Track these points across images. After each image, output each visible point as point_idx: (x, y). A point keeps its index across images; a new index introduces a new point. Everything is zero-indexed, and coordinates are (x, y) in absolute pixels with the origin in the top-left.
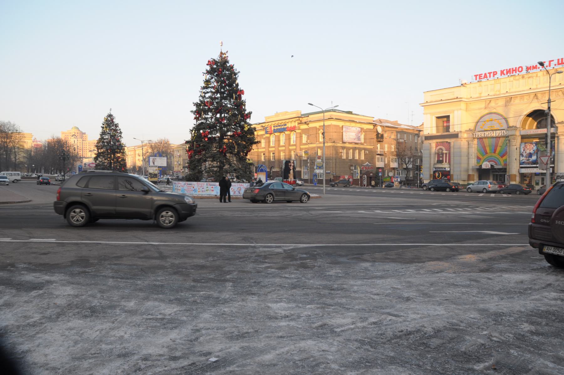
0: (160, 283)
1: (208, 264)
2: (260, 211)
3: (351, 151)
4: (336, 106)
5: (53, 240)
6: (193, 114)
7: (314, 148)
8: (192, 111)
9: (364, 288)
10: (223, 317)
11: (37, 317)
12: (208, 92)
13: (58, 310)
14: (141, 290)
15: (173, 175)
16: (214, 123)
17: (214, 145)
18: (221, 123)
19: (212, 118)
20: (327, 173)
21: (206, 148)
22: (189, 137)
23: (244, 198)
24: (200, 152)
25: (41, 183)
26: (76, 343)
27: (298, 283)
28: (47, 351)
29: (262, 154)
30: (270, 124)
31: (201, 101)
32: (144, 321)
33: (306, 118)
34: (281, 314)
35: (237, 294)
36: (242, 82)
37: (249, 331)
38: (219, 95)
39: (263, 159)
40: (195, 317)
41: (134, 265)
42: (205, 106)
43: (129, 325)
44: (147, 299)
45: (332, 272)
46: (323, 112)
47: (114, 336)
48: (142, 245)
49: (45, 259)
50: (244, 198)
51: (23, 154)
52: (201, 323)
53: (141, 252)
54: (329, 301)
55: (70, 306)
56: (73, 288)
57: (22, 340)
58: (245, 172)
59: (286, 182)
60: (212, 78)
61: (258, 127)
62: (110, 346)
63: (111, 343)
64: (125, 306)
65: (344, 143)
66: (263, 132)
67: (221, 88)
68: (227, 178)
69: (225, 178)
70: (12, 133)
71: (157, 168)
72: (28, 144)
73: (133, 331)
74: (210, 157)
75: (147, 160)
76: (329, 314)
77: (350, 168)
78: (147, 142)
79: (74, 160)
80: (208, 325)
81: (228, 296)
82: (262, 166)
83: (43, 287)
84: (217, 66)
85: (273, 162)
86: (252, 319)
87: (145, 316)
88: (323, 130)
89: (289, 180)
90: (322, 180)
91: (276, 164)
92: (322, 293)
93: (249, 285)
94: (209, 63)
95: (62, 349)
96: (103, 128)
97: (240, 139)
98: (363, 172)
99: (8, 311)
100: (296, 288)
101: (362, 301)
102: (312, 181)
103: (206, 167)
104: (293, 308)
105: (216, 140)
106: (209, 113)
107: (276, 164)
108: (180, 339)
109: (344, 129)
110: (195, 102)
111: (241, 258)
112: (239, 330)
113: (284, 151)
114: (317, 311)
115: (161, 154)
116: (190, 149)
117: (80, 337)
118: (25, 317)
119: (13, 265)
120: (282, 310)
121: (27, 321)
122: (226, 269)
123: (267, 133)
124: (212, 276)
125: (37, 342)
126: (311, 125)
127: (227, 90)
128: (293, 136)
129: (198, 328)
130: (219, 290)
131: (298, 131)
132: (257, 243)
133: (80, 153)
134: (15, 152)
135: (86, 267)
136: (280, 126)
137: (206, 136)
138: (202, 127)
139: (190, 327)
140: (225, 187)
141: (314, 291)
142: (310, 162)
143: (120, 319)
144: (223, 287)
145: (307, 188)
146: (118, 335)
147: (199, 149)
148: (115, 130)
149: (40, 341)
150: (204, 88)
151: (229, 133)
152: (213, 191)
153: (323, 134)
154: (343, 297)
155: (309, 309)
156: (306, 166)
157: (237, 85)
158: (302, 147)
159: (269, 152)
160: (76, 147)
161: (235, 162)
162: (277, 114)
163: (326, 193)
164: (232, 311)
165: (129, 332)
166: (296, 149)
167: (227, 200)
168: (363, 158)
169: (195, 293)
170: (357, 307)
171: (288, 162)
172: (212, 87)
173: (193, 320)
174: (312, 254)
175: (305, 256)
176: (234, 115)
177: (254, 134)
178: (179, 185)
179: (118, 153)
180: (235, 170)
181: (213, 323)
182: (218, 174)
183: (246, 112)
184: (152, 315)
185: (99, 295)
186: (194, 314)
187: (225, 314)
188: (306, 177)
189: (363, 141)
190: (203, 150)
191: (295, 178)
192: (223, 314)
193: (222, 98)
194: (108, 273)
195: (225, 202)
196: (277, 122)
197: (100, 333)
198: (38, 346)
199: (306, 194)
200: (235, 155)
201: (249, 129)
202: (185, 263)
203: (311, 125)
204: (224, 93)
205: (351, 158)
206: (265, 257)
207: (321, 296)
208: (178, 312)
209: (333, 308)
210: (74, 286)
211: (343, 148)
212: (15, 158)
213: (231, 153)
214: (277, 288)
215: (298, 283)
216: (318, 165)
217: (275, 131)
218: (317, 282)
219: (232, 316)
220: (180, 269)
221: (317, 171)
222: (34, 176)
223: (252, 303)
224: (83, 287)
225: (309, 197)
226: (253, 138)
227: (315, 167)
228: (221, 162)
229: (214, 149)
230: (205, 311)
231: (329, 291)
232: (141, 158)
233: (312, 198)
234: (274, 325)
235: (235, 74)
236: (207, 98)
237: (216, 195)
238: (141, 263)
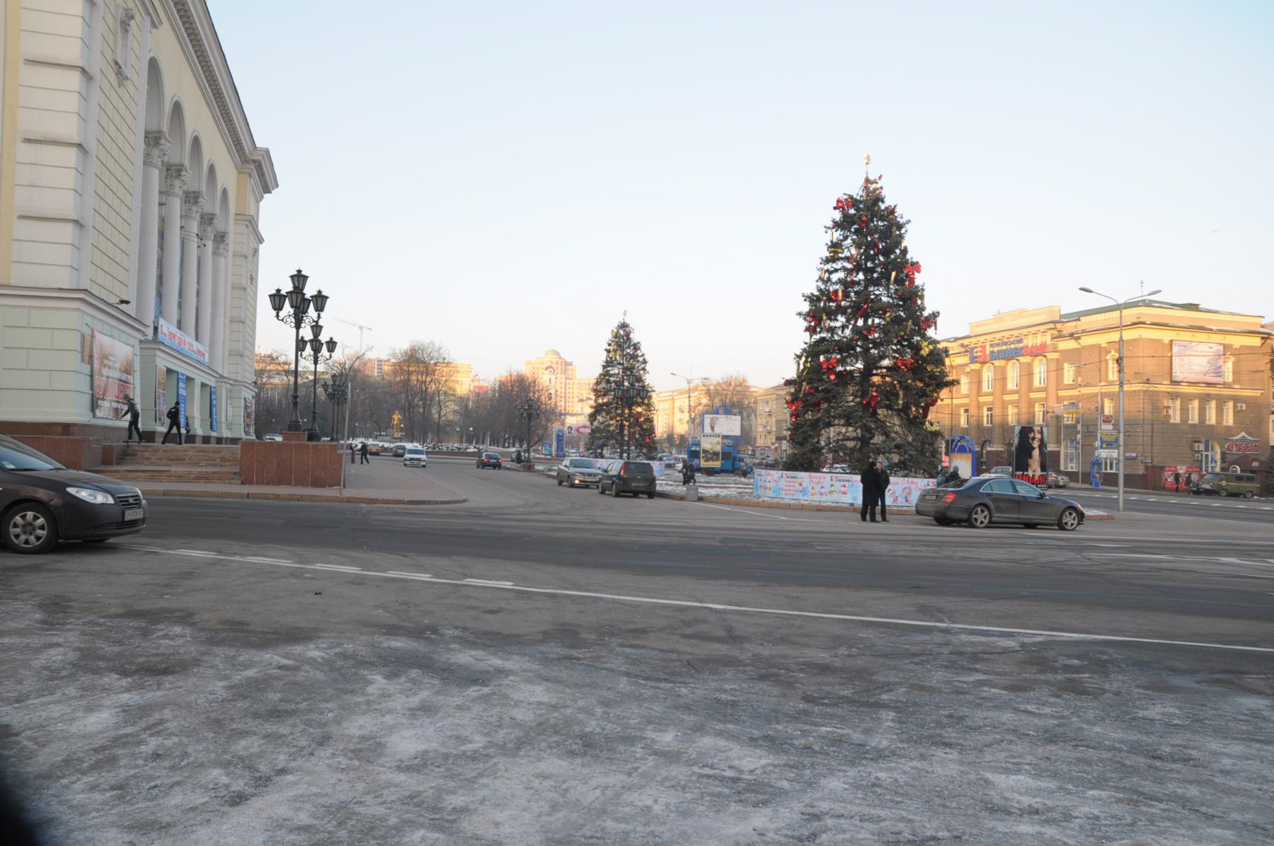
0: (729, 698)
1: (838, 663)
2: (957, 544)
3: (1196, 403)
4: (1154, 293)
5: (508, 585)
6: (801, 320)
7: (1095, 395)
8: (800, 314)
9: (1254, 766)
10: (874, 793)
11: (479, 742)
12: (836, 270)
13: (519, 733)
14: (687, 708)
15: (753, 455)
16: (852, 339)
17: (851, 389)
18: (865, 339)
19: (844, 327)
20: (1127, 459)
21: (831, 396)
22: (791, 371)
23: (918, 512)
24: (816, 405)
25: (483, 465)
26: (554, 807)
27: (1061, 730)
28: (500, 816)
29: (962, 410)
30: (982, 339)
31: (820, 290)
32: (694, 778)
33: (1074, 324)
34: (1018, 802)
35: (908, 741)
36: (915, 245)
37: (940, 834)
38: (861, 276)
39: (963, 422)
40: (810, 784)
41: (672, 651)
42: (830, 300)
43: (662, 783)
44: (700, 729)
45: (1154, 712)
46: (1118, 307)
47: (631, 804)
48: (688, 608)
49: (493, 623)
50: (918, 512)
51: (453, 406)
52: (823, 799)
53: (688, 624)
54: (1148, 786)
55: (541, 727)
56: (547, 690)
57: (453, 784)
58: (922, 454)
59: (1022, 477)
60: (846, 238)
61: (954, 348)
62: (623, 825)
63: (624, 820)
64: (654, 741)
65: (1174, 383)
66: (964, 360)
67: (867, 260)
68: (878, 466)
69: (874, 464)
70: (435, 364)
71: (720, 439)
72: (463, 386)
73: (672, 798)
74: (840, 417)
75: (697, 421)
76: (1152, 822)
77: (1191, 447)
78: (699, 382)
79: (548, 420)
80: (839, 808)
81: (885, 743)
82: (962, 438)
83: (489, 680)
84: (858, 210)
85: (988, 429)
86: (945, 806)
87: (696, 769)
88: (1119, 351)
89: (1030, 473)
90: (1116, 475)
91: (997, 435)
92: (1128, 762)
93: (937, 723)
94: (840, 205)
95: (527, 816)
96: (608, 351)
97: (910, 375)
98: (1229, 458)
99: (428, 721)
100: (1056, 743)
101: (1252, 802)
102: (1086, 478)
103: (829, 438)
104: (1051, 792)
105: (853, 377)
106: (839, 317)
107: (997, 435)
108: (776, 831)
109: (1175, 349)
110: (808, 292)
111: (915, 655)
112: (913, 829)
113: (1016, 404)
114: (1117, 809)
115: (728, 409)
116: (794, 399)
117: (562, 796)
118: (458, 738)
119: (434, 630)
120: (1021, 794)
121: (462, 748)
122: (880, 678)
123: (973, 360)
124: (846, 693)
125: (481, 794)
126: (1086, 341)
127: (881, 263)
128: (1040, 369)
129: (815, 810)
130: (864, 725)
131: (1051, 356)
132: (954, 622)
133: (561, 405)
134: (439, 402)
135: (573, 647)
136: (1006, 344)
137: (831, 370)
138: (822, 347)
139: (798, 806)
140: (875, 486)
141: (1105, 755)
142: (1084, 430)
143: (644, 767)
144: (873, 719)
145: (1075, 495)
146: (640, 804)
147: (814, 399)
148: (634, 357)
149: (485, 792)
150: (827, 261)
151: (886, 362)
152: (844, 493)
153: (1119, 361)
154: (1191, 782)
155: (1095, 799)
156: (1072, 441)
157: (905, 252)
158: (1062, 393)
159: (979, 406)
160: (552, 391)
161: (897, 428)
162: (999, 317)
163: (1125, 509)
164: (896, 780)
165: (662, 800)
166: (1046, 399)
167: (878, 517)
168: (1229, 420)
169: (808, 727)
170: (1235, 816)
171: (1026, 431)
172: (848, 259)
173: (805, 791)
174: (1098, 660)
175: (1076, 662)
176: (897, 321)
177: (944, 364)
178: (769, 478)
179: (639, 405)
180: (897, 447)
181: (851, 803)
182: (856, 455)
183: (926, 314)
184: (712, 767)
185: (599, 711)
186: (807, 778)
187: (879, 786)
188: (1072, 467)
189: (1229, 378)
190: (827, 400)
191: (1043, 468)
192: (874, 785)
193: (870, 282)
194: (618, 663)
195: (873, 520)
196: (998, 336)
197: (603, 794)
198: (482, 802)
199: (1074, 509)
200: (899, 411)
201: (931, 353)
202: (784, 657)
203: (1086, 341)
204: (872, 270)
205: (1196, 421)
206: (975, 657)
207: (1126, 771)
208: (771, 768)
209: (1162, 806)
210: (549, 685)
211: (1173, 396)
212: (439, 413)
213: (889, 407)
214: (1008, 737)
215: (1061, 730)
216: (1106, 438)
217: (994, 356)
218: (1114, 734)
219: (897, 793)
220: (774, 670)
221: (1103, 453)
222: (472, 450)
223: (945, 766)
224: (567, 691)
225: (1081, 516)
226: (944, 374)
227: (1098, 444)
228: (865, 428)
229: (850, 399)
230: (831, 772)
231: (1148, 761)
232: (686, 416)
233: (1090, 518)
234: (1001, 827)
235: (900, 227)
236: (836, 283)
237: (852, 505)
238: (688, 649)
